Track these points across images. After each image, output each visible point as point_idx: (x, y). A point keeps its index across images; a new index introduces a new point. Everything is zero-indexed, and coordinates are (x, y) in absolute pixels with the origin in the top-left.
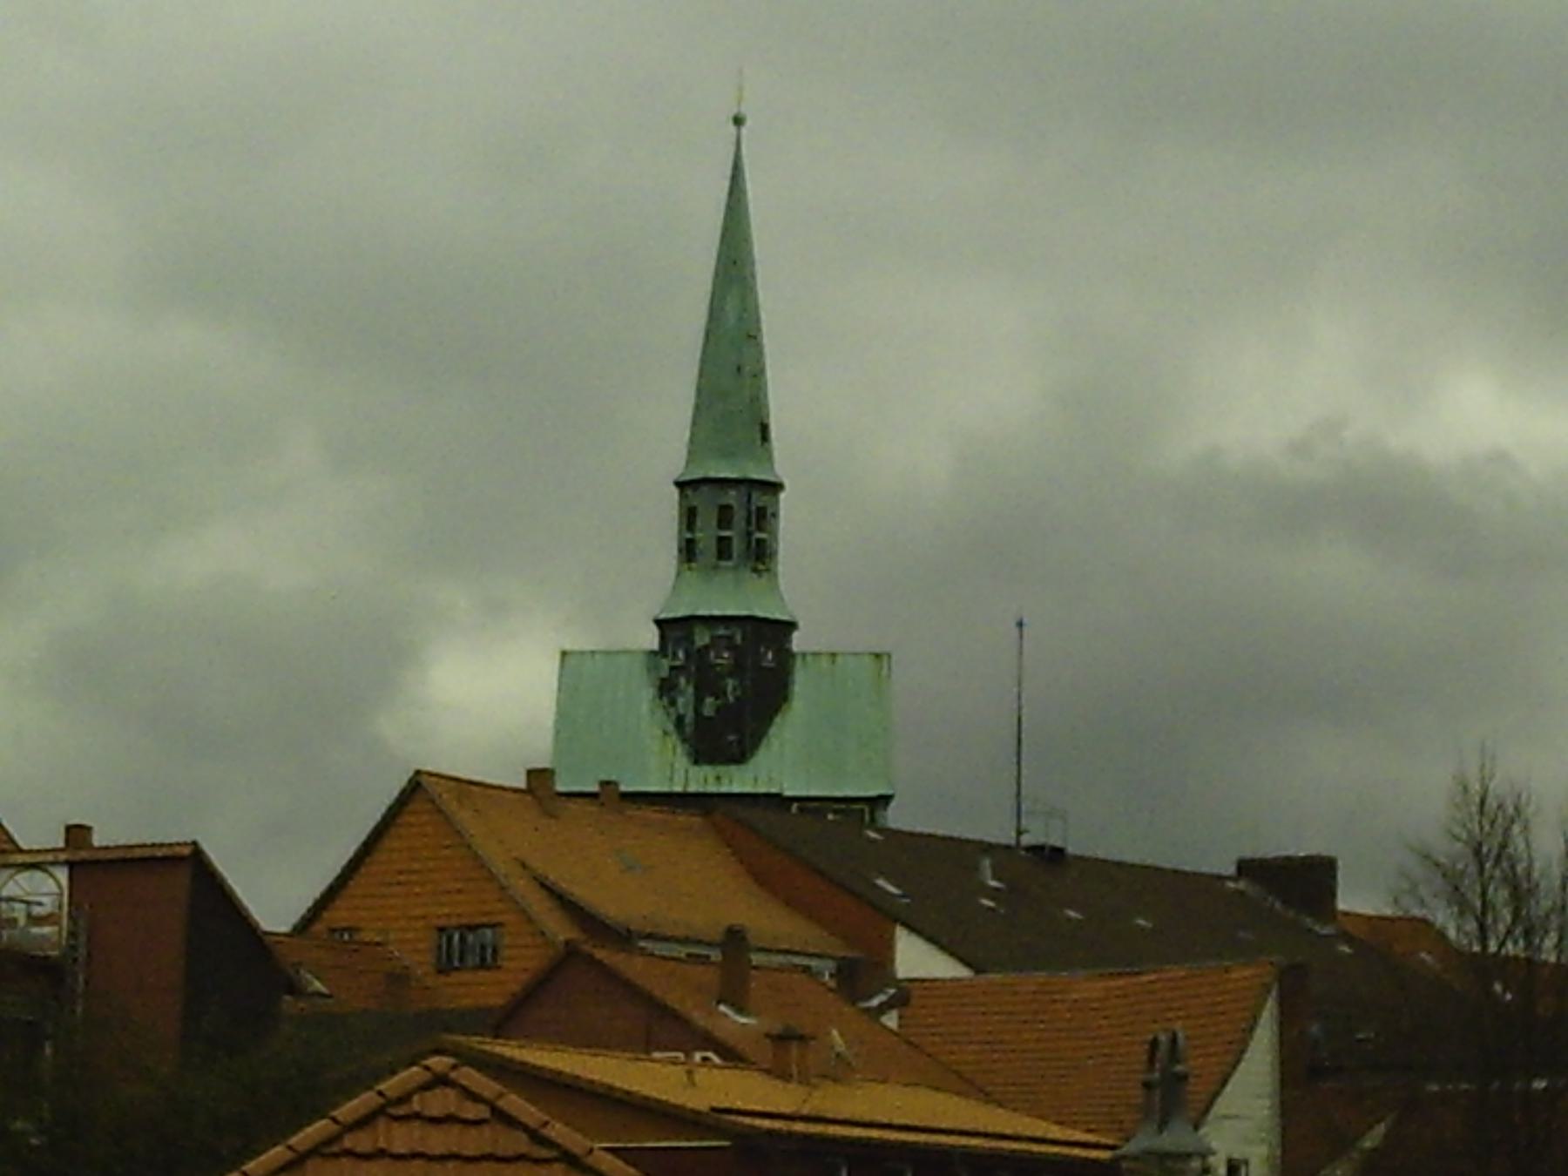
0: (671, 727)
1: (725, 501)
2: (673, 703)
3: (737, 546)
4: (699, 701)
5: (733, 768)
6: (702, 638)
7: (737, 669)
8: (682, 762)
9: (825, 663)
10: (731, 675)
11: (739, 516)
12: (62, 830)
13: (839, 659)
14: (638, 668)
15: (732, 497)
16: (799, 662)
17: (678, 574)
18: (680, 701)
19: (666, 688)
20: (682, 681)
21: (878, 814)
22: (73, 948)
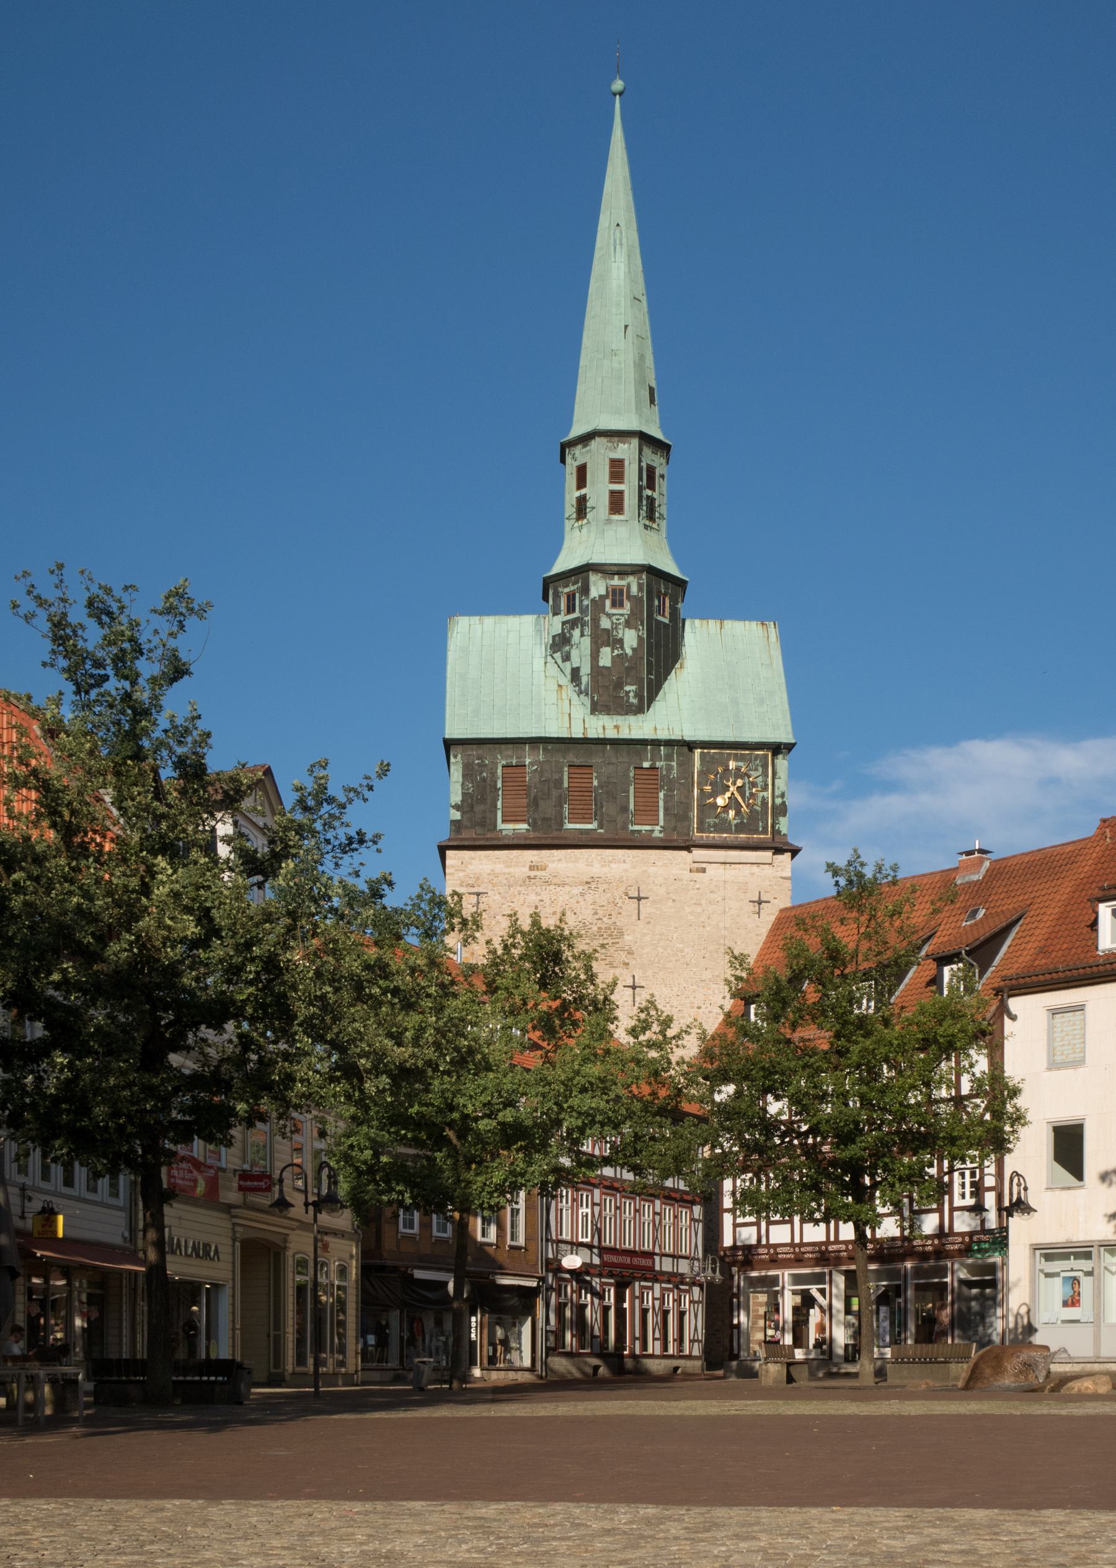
0: (565, 681)
2: (567, 658)
3: (630, 501)
4: (595, 656)
6: (598, 587)
8: (580, 708)
10: (628, 624)
18: (574, 653)
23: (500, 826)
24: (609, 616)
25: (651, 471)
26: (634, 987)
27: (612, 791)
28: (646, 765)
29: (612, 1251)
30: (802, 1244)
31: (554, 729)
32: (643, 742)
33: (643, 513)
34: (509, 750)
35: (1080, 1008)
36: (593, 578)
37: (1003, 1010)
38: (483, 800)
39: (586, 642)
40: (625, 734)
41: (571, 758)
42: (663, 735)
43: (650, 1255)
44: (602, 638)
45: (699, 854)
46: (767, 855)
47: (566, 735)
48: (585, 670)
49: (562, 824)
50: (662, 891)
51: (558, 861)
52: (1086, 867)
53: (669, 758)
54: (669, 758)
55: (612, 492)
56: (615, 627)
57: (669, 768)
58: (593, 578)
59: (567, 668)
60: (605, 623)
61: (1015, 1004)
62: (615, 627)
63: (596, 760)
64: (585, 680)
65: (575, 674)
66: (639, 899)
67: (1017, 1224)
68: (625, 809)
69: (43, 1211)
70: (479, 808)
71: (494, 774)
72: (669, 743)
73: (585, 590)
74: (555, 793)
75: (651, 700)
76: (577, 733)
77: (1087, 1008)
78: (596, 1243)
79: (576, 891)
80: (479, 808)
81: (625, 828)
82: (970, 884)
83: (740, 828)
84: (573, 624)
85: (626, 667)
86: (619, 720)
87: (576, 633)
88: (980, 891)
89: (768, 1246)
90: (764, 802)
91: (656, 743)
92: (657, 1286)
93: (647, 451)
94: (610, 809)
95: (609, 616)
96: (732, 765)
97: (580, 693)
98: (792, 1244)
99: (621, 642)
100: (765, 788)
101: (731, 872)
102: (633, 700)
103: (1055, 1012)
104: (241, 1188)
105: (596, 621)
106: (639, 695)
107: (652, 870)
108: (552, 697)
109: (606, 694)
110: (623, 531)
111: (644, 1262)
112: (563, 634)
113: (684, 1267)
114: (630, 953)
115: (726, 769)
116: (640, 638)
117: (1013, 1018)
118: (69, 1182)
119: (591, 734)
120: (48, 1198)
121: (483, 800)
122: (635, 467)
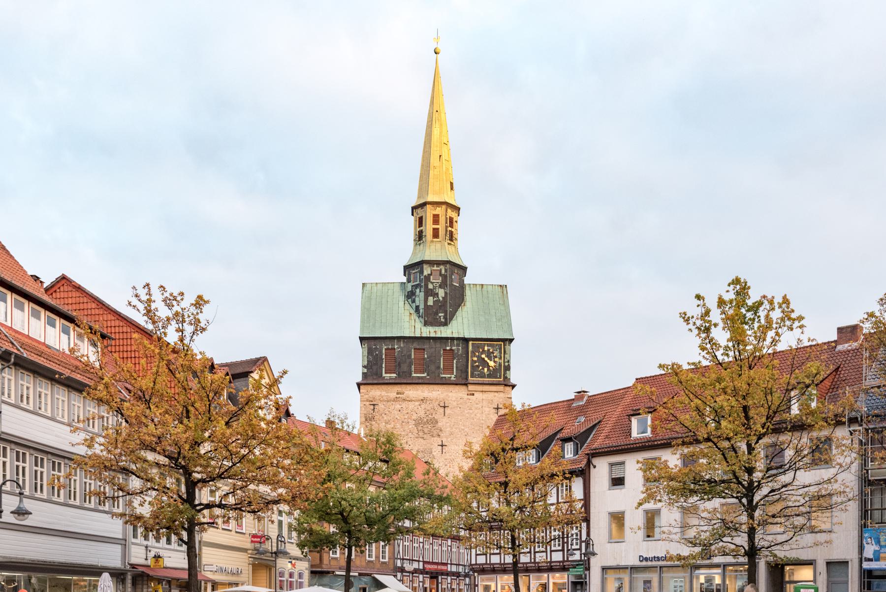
0: (413, 311)
1: (436, 213)
2: (414, 301)
3: (442, 233)
4: (426, 300)
5: (442, 328)
6: (427, 270)
7: (443, 285)
8: (419, 324)
9: (479, 288)
10: (440, 287)
11: (442, 220)
12: (59, 275)
13: (485, 287)
14: (397, 288)
15: (439, 211)
16: (467, 288)
17: (415, 249)
18: (417, 299)
19: (410, 296)
20: (418, 290)
21: (507, 347)
22: (337, 520)
23: (384, 375)
24: (432, 283)
25: (451, 219)
26: (442, 446)
27: (434, 360)
28: (448, 348)
29: (428, 563)
30: (504, 564)
31: (407, 333)
32: (447, 339)
33: (447, 238)
34: (388, 342)
35: (623, 463)
36: (425, 266)
37: (589, 463)
38: (376, 364)
39: (422, 294)
40: (439, 335)
41: (416, 345)
42: (455, 335)
43: (446, 564)
44: (429, 293)
45: (471, 387)
46: (501, 388)
47: (413, 335)
48: (422, 307)
49: (411, 374)
50: (455, 404)
51: (412, 392)
52: (628, 400)
53: (458, 345)
54: (458, 345)
55: (434, 229)
56: (435, 288)
57: (458, 350)
58: (425, 266)
59: (414, 305)
60: (430, 286)
61: (595, 461)
62: (435, 288)
63: (426, 346)
64: (421, 311)
65: (417, 308)
66: (444, 407)
67: (593, 560)
68: (439, 367)
69: (155, 557)
70: (375, 368)
71: (381, 352)
72: (458, 339)
73: (422, 272)
74: (408, 361)
75: (451, 319)
76: (418, 335)
77: (626, 464)
78: (421, 559)
79: (417, 403)
80: (375, 368)
81: (439, 376)
82: (579, 406)
83: (489, 376)
84: (416, 286)
85: (441, 306)
86: (437, 328)
87: (418, 290)
88: (582, 410)
89: (490, 564)
90: (500, 365)
91: (452, 339)
92: (449, 578)
93: (449, 210)
94: (432, 368)
95: (432, 283)
96: (486, 348)
97: (419, 317)
98: (500, 564)
99: (437, 294)
100: (500, 358)
101: (485, 396)
102: (442, 320)
103: (612, 465)
104: (252, 542)
105: (426, 285)
106: (445, 318)
107: (450, 394)
108: (407, 318)
109: (430, 317)
110: (438, 246)
111: (444, 568)
112: (412, 291)
113: (461, 569)
114: (441, 430)
115: (483, 350)
116: (446, 293)
117: (595, 467)
118: (169, 541)
119: (424, 335)
120: (157, 550)
121: (376, 364)
122: (444, 218)
